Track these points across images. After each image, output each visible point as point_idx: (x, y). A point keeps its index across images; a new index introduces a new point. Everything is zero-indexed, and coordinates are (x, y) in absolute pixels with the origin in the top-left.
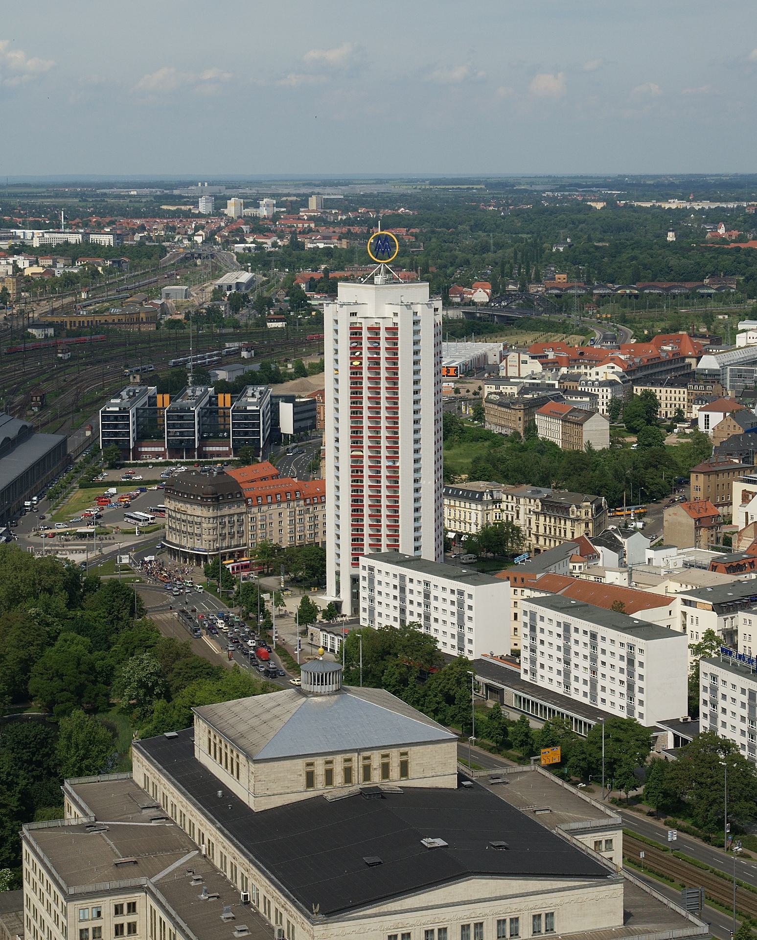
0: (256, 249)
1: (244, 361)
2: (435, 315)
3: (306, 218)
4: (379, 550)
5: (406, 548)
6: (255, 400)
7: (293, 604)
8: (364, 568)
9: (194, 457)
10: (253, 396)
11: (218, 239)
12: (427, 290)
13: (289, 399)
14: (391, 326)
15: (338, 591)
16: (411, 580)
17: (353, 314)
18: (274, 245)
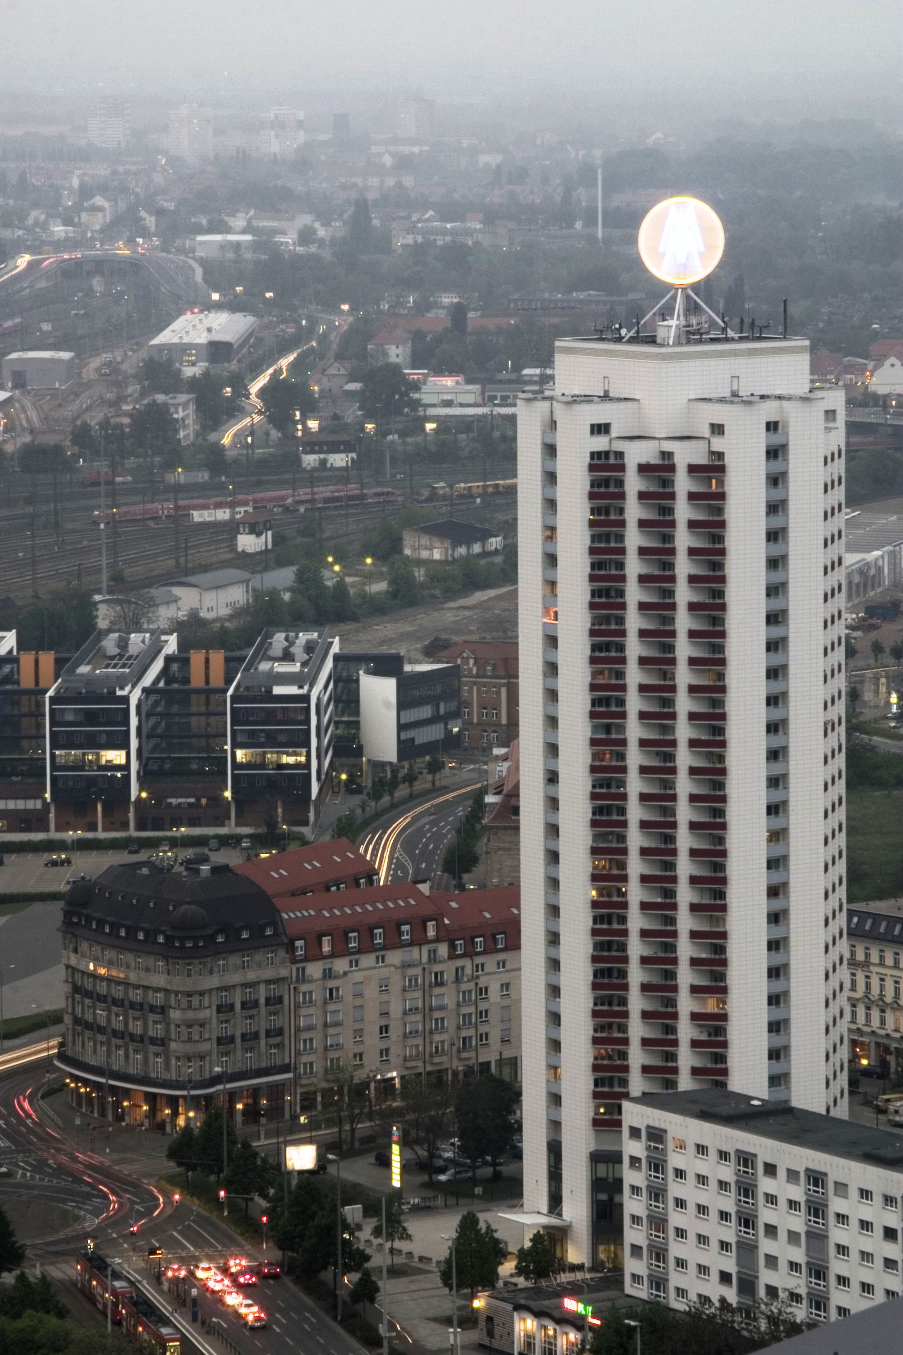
0: (256, 246)
1: (248, 562)
2: (828, 430)
3: (388, 161)
4: (671, 1084)
5: (748, 1075)
6: (296, 668)
7: (433, 1236)
8: (635, 1133)
9: (125, 826)
10: (287, 656)
11: (150, 221)
12: (804, 360)
13: (387, 665)
14: (655, 460)
15: (555, 1201)
16: (771, 1170)
17: (600, 429)
18: (306, 236)
